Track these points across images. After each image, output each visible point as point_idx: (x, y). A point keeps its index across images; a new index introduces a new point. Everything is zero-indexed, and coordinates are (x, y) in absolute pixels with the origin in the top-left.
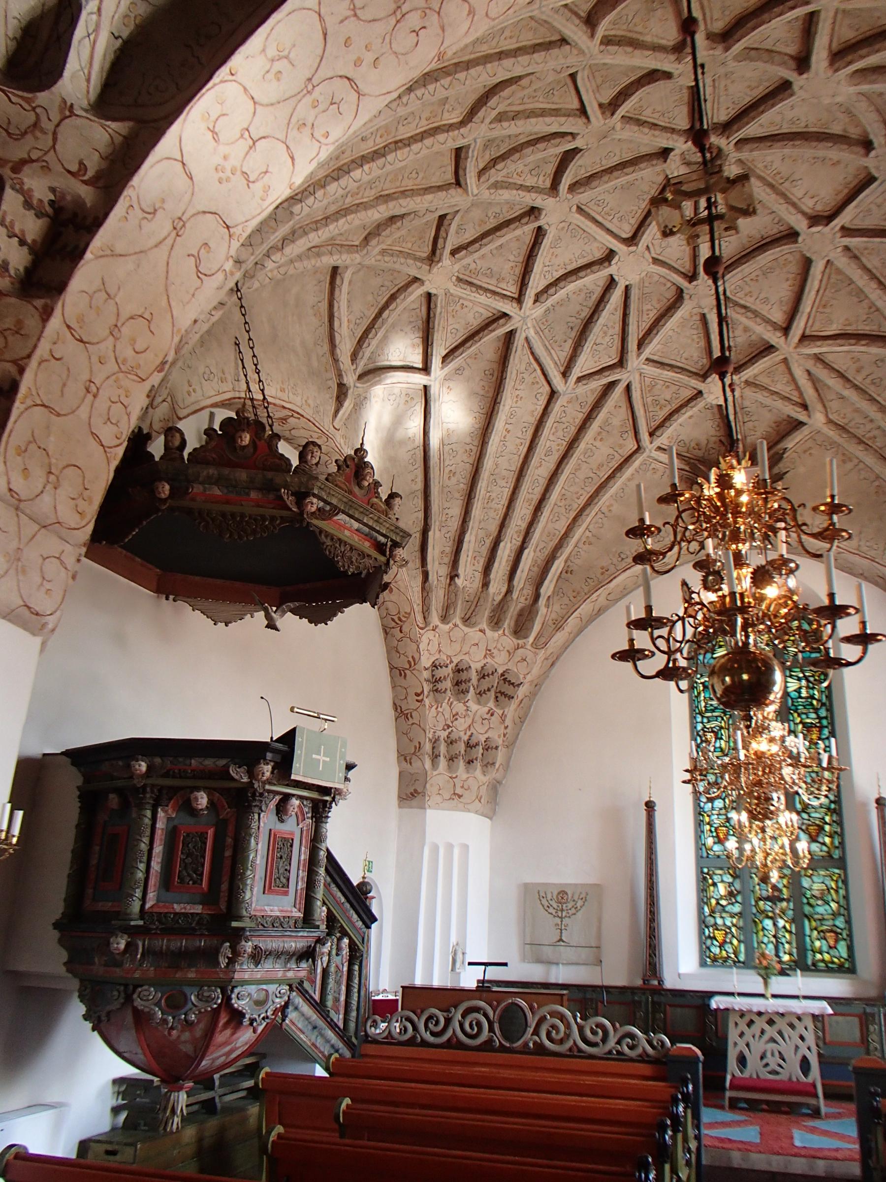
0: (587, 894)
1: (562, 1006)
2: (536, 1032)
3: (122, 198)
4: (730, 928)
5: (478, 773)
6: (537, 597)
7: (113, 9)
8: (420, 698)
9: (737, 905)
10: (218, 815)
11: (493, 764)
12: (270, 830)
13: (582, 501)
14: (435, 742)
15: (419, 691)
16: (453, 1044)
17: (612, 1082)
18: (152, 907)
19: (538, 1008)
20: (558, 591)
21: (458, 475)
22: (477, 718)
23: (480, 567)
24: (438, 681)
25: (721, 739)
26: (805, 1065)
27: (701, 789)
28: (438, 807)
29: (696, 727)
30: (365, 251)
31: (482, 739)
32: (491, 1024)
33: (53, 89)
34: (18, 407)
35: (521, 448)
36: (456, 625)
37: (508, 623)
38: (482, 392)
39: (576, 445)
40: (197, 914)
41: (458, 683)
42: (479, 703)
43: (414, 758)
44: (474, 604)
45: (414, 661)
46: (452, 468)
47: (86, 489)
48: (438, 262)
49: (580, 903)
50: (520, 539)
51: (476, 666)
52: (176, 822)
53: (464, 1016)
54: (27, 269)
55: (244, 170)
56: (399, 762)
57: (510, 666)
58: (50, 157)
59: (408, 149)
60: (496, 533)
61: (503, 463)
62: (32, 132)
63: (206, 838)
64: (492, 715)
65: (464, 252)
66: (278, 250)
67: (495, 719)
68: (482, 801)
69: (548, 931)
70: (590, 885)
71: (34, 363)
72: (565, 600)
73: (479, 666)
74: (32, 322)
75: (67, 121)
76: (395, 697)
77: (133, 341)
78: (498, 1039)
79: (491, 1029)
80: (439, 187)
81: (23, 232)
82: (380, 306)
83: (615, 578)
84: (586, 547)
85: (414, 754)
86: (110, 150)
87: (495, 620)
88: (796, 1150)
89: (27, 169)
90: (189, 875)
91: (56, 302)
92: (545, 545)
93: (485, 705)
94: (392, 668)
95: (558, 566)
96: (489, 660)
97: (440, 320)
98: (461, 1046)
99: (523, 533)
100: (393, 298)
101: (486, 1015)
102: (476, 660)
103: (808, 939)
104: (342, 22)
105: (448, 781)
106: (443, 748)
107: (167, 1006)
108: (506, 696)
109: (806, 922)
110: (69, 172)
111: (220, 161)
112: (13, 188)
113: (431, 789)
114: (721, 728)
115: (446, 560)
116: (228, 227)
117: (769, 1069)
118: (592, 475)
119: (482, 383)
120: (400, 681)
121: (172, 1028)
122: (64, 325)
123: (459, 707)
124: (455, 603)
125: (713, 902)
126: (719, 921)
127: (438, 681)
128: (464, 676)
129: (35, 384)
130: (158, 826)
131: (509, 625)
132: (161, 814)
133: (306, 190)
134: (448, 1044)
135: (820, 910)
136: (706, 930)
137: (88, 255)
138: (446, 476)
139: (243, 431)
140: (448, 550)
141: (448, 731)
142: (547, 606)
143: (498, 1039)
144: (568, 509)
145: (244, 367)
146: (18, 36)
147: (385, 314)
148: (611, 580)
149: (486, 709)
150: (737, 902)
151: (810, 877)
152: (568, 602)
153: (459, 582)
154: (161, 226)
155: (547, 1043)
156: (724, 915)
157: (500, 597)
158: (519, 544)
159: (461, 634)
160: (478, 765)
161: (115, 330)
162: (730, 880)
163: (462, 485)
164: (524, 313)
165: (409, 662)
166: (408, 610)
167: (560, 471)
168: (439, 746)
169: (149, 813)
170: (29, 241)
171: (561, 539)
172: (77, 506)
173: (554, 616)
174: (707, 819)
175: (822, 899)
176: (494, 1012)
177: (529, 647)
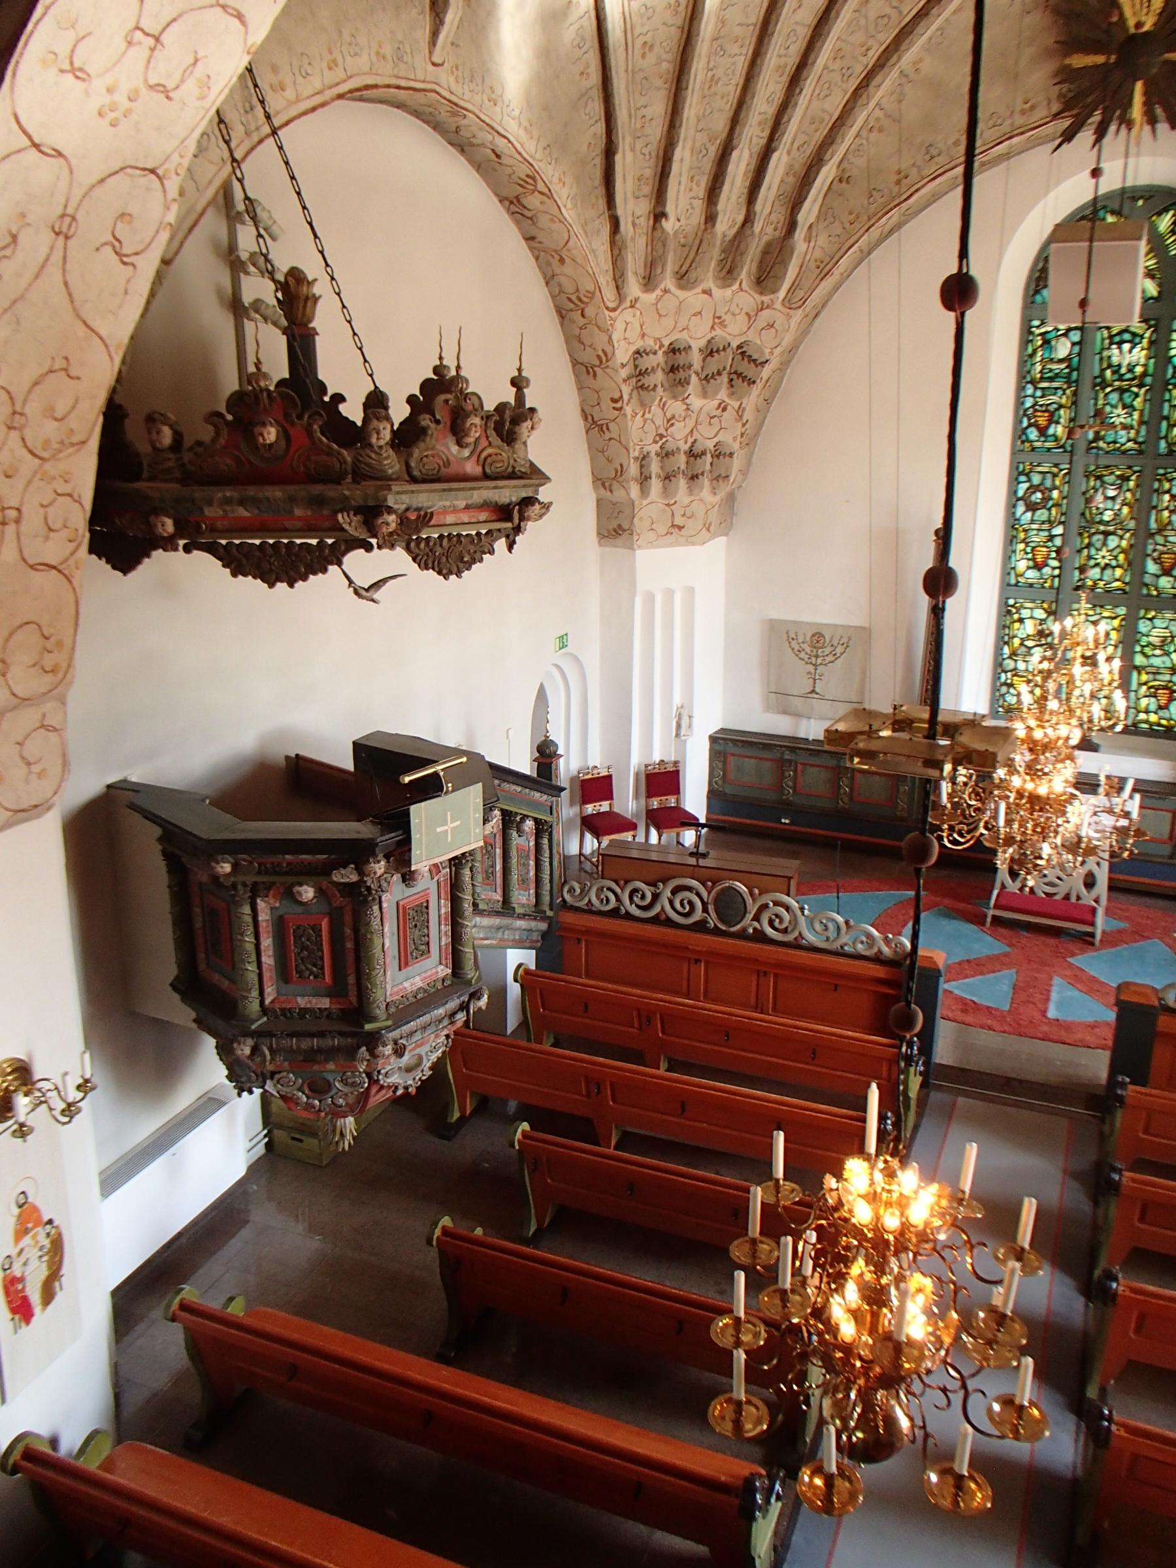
1: (788, 895)
2: (756, 918)
5: (706, 494)
6: (792, 226)
8: (618, 405)
10: (330, 904)
11: (727, 477)
12: (398, 903)
14: (643, 459)
15: (617, 396)
16: (661, 921)
18: (272, 1002)
19: (760, 894)
20: (823, 213)
21: (657, 49)
22: (703, 418)
23: (701, 191)
25: (1057, 423)
26: (1090, 882)
27: (1020, 493)
28: (651, 545)
29: (1023, 403)
31: (710, 445)
32: (704, 904)
36: (666, 291)
40: (326, 1009)
41: (673, 369)
42: (705, 394)
43: (615, 485)
44: (694, 249)
45: (606, 355)
46: (648, 38)
49: (839, 650)
50: (766, 133)
51: (697, 345)
52: (281, 912)
53: (674, 892)
55: (152, 82)
56: (595, 488)
57: (751, 336)
60: (724, 135)
61: (735, 16)
63: (321, 930)
64: (724, 409)
67: (729, 415)
68: (712, 528)
69: (798, 677)
70: (856, 627)
72: (837, 229)
73: (702, 343)
76: (583, 402)
78: (713, 920)
79: (705, 910)
83: (917, 191)
85: (614, 479)
87: (727, 267)
88: (1045, 1028)
90: (307, 969)
92: (806, 138)
94: (575, 363)
95: (827, 174)
96: (718, 332)
98: (669, 922)
99: (770, 124)
101: (698, 895)
105: (664, 510)
106: (655, 467)
107: (311, 1090)
108: (744, 378)
109: (1135, 674)
111: (106, 100)
113: (640, 524)
114: (1061, 406)
115: (647, 189)
116: (153, 171)
117: (1046, 880)
118: (888, 11)
120: (589, 381)
121: (320, 1110)
123: (676, 407)
124: (663, 258)
125: (1016, 642)
126: (1021, 666)
128: (681, 359)
130: (260, 919)
131: (749, 274)
132: (261, 904)
134: (655, 920)
138: (638, 52)
139: (264, 424)
140: (648, 173)
141: (660, 443)
142: (808, 239)
143: (713, 920)
144: (846, 74)
145: (256, 86)
149: (716, 403)
151: (1151, 619)
152: (839, 231)
153: (669, 225)
155: (769, 931)
157: (735, 230)
158: (763, 142)
159: (676, 303)
160: (706, 482)
162: (1044, 616)
165: (598, 357)
166: (591, 287)
167: (833, 14)
168: (649, 465)
169: (247, 909)
171: (832, 129)
172: (43, 669)
173: (818, 254)
174: (1022, 535)
175: (1161, 647)
176: (709, 893)
177: (778, 305)
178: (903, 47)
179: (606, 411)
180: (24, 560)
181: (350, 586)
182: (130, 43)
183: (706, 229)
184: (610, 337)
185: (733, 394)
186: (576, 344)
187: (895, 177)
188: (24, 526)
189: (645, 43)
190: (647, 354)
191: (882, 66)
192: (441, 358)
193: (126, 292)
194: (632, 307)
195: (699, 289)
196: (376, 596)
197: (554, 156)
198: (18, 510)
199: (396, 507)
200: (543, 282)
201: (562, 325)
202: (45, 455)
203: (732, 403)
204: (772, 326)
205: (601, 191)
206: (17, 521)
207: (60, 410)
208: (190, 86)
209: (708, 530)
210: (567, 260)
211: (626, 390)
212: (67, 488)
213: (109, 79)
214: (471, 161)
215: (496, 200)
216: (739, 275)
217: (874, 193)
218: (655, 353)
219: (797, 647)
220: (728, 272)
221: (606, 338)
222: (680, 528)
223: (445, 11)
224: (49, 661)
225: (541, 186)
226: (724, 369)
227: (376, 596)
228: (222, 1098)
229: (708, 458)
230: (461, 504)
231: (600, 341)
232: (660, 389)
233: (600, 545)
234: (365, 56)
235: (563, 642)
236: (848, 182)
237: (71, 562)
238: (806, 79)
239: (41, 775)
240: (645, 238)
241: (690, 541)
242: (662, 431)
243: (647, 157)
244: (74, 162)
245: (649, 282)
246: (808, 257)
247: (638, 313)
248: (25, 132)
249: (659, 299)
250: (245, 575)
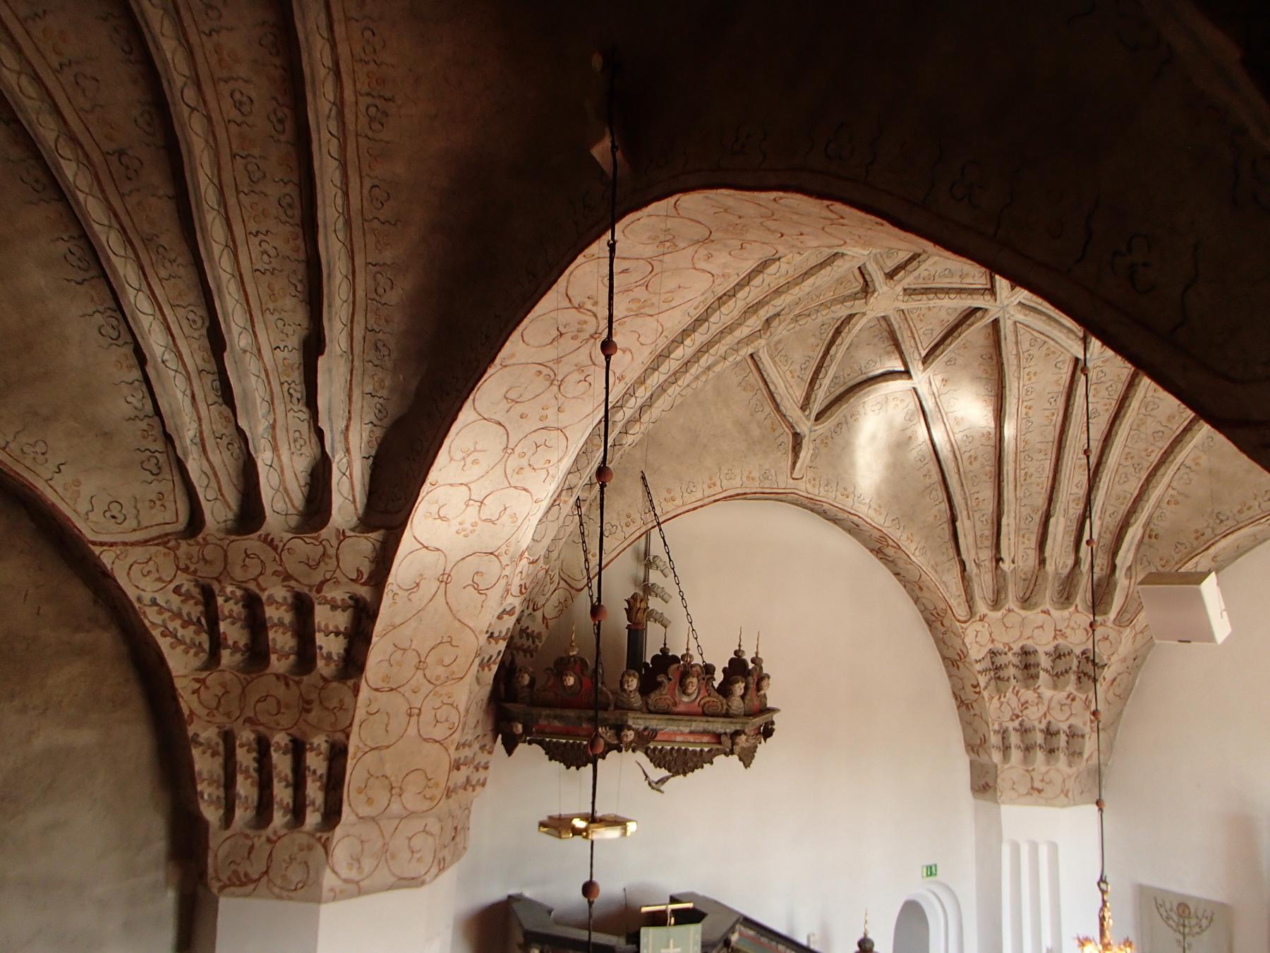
0: (1213, 913)
3: (385, 595)
7: (358, 442)
8: (977, 690)
11: (1081, 754)
13: (1155, 457)
14: (1004, 733)
15: (975, 683)
21: (980, 458)
24: (998, 669)
28: (1012, 802)
30: (768, 334)
31: (1064, 726)
33: (329, 525)
34: (350, 763)
35: (1054, 418)
36: (1009, 610)
37: (1083, 595)
38: (986, 376)
39: (1127, 404)
41: (1027, 667)
42: (1055, 687)
46: (972, 453)
47: (430, 780)
48: (874, 291)
54: (346, 650)
58: (338, 573)
59: (734, 299)
62: (323, 560)
64: (1073, 700)
65: (903, 272)
66: (636, 421)
68: (1070, 795)
71: (355, 728)
74: (348, 699)
75: (343, 543)
76: (953, 686)
77: (441, 662)
80: (821, 264)
81: (337, 627)
82: (826, 342)
84: (1172, 506)
86: (374, 555)
87: (1065, 595)
89: (325, 588)
91: (360, 680)
93: (1063, 689)
94: (944, 658)
95: (1134, 533)
96: (1060, 641)
97: (902, 333)
100: (838, 332)
102: (1043, 644)
104: (508, 411)
106: (1014, 739)
110: (352, 580)
112: (320, 604)
115: (988, 543)
118: (1162, 429)
119: (982, 367)
122: (373, 691)
123: (1028, 695)
124: (1005, 588)
127: (998, 669)
128: (1032, 659)
129: (361, 740)
133: (626, 393)
137: (374, 639)
140: (987, 533)
146: (309, 481)
147: (832, 351)
148: (1209, 547)
149: (1065, 694)
154: (429, 587)
160: (1062, 758)
161: (421, 665)
163: (988, 468)
164: (1001, 302)
166: (944, 606)
168: (1008, 738)
170: (342, 630)
172: (425, 796)
178: (1176, 451)
179: (969, 695)
180: (420, 735)
181: (646, 779)
182: (467, 505)
183: (1040, 569)
184: (963, 641)
185: (1080, 688)
186: (942, 644)
187: (1193, 536)
188: (421, 718)
189: (971, 456)
190: (1000, 654)
191: (1164, 462)
192: (740, 646)
193: (482, 606)
194: (981, 620)
195: (1039, 610)
196: (662, 788)
197: (902, 525)
198: (420, 710)
199: (634, 726)
200: (913, 604)
201: (931, 631)
202: (438, 683)
203: (1080, 695)
204: (1107, 639)
205: (951, 544)
206: (419, 715)
207: (447, 661)
208: (505, 518)
209: (1066, 795)
210: (924, 588)
211: (982, 680)
212: (450, 701)
213: (460, 519)
214: (844, 529)
215: (868, 551)
216: (1074, 600)
217: (1179, 546)
218: (1006, 654)
219: (1165, 914)
220: (1066, 595)
221: (961, 641)
222: (1040, 791)
223: (800, 451)
224: (429, 793)
225: (891, 542)
226: (1070, 668)
227: (662, 788)
229: (1063, 738)
230: (687, 730)
231: (957, 643)
232: (1013, 681)
233: (975, 797)
234: (738, 479)
235: (931, 871)
236: (1155, 538)
237: (449, 740)
238: (1103, 472)
239: (419, 860)
240: (991, 574)
241: (1049, 802)
242: (1017, 712)
243: (985, 523)
244: (447, 553)
245: (996, 604)
246: (1131, 590)
247: (987, 625)
248: (419, 542)
249: (1004, 616)
250: (556, 760)
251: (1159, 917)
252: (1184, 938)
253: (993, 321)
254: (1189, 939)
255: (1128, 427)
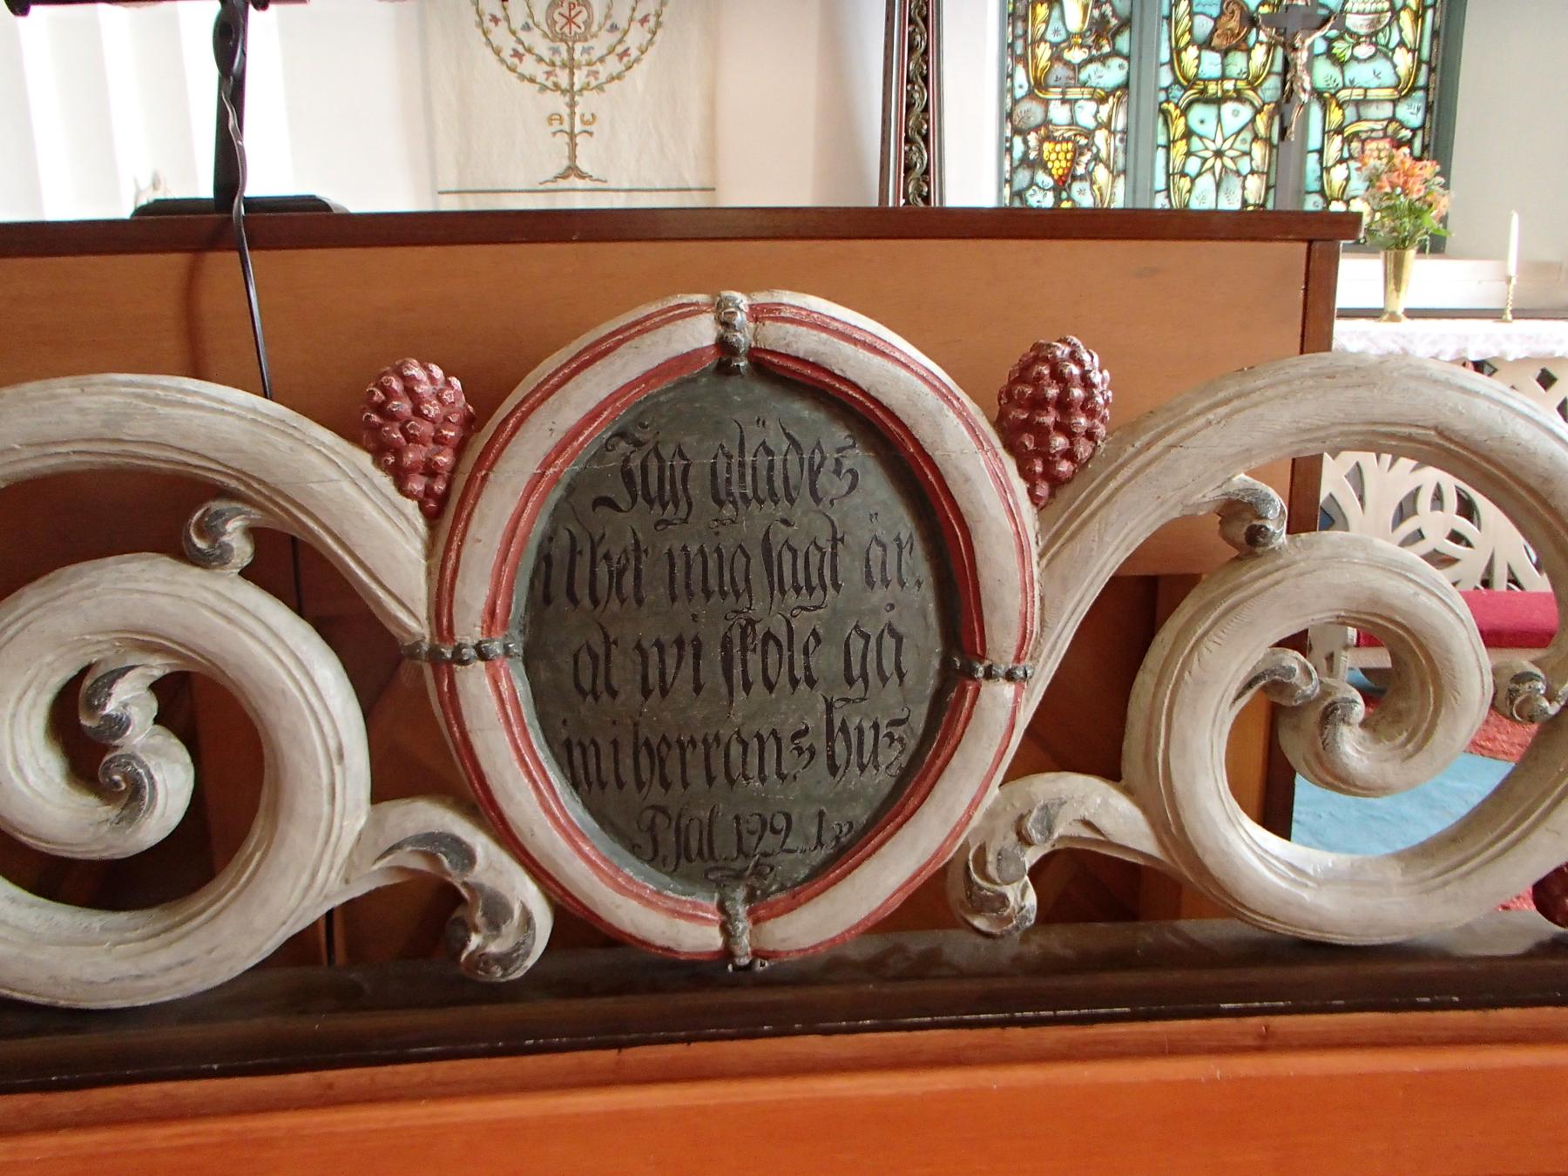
4: (1089, 134)
9: (1115, 62)
17: (1499, 825)
49: (636, 38)
103: (1312, 159)
125: (1044, 52)
126: (1059, 114)
135: (1359, 73)
136: (1018, 140)
150: (1115, 53)
156: (1073, 93)
228: (1189, 571)
251: (493, 58)
252: (572, 105)
253: (1488, 644)
254: (584, 104)
255: (618, 898)
